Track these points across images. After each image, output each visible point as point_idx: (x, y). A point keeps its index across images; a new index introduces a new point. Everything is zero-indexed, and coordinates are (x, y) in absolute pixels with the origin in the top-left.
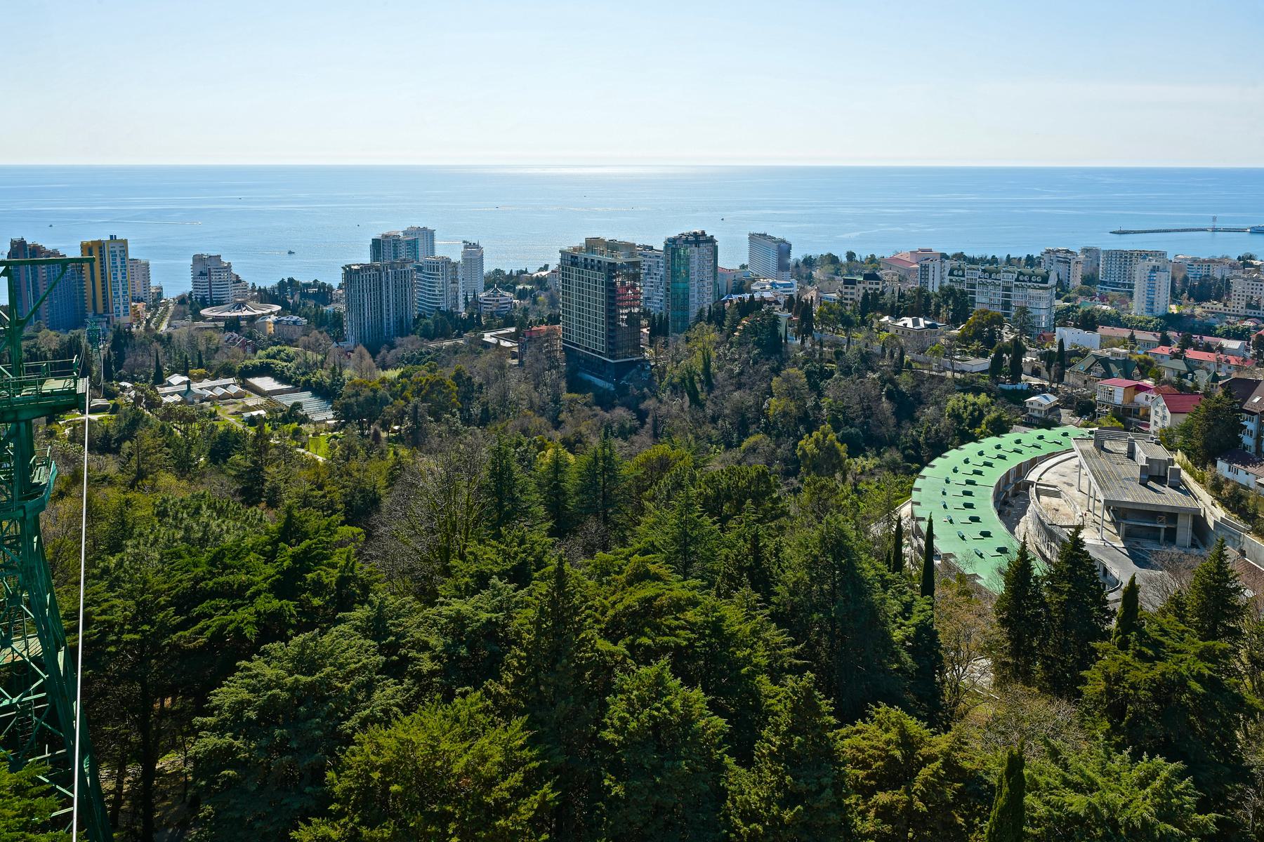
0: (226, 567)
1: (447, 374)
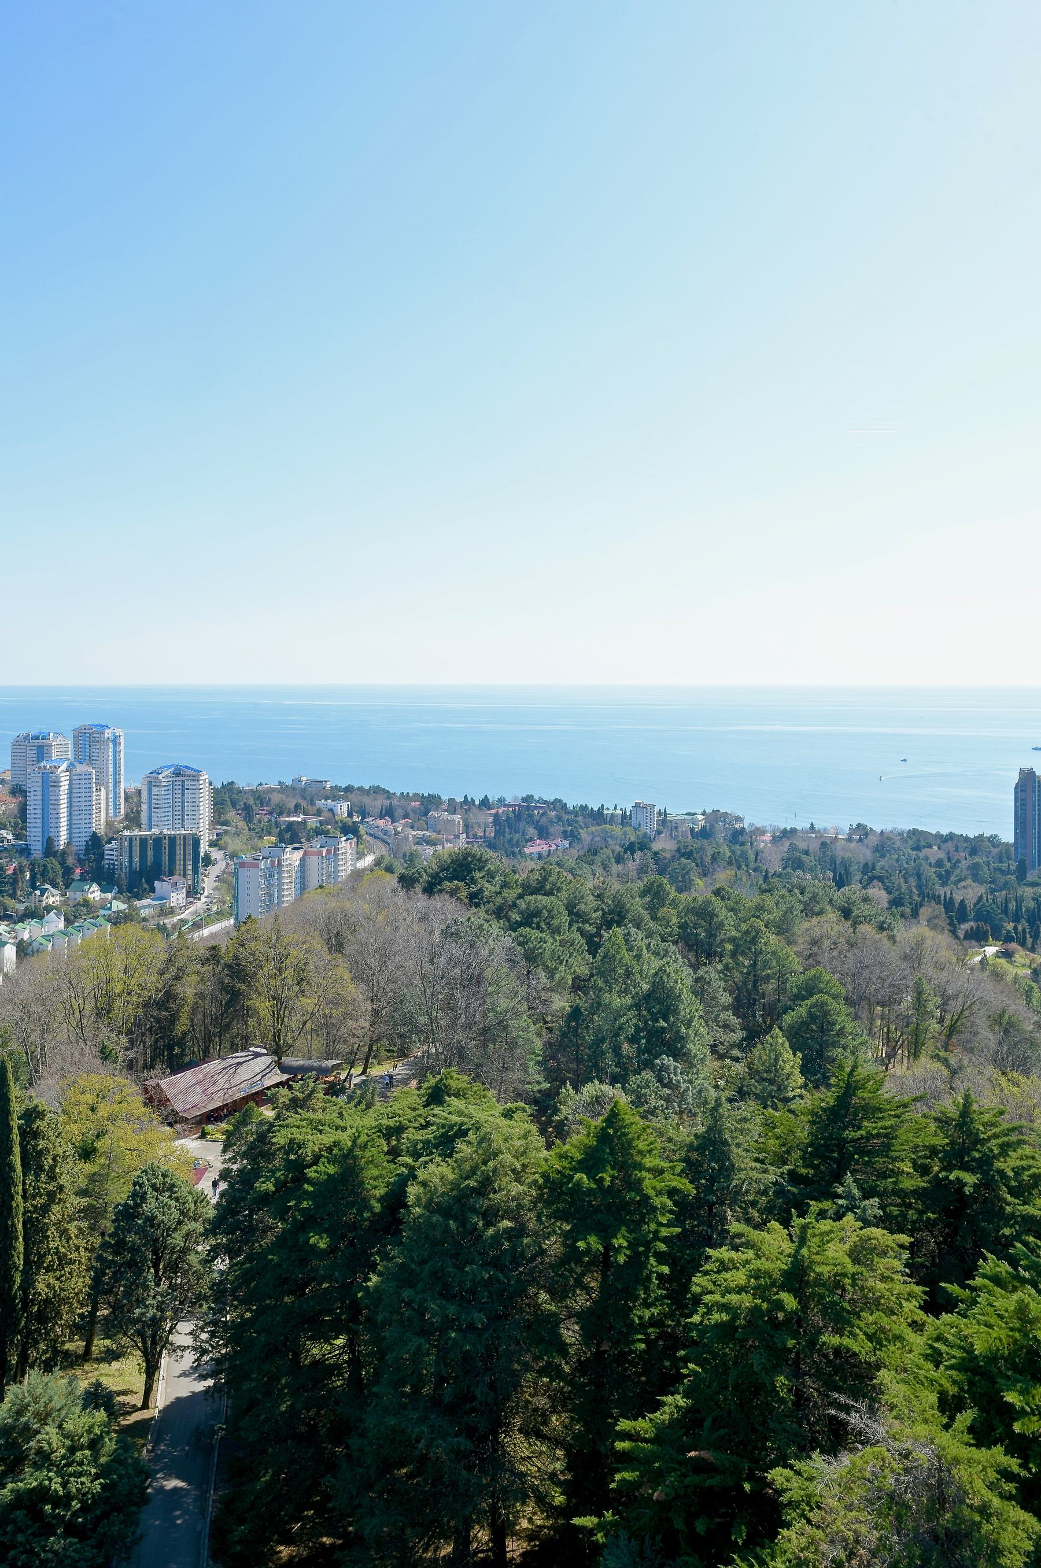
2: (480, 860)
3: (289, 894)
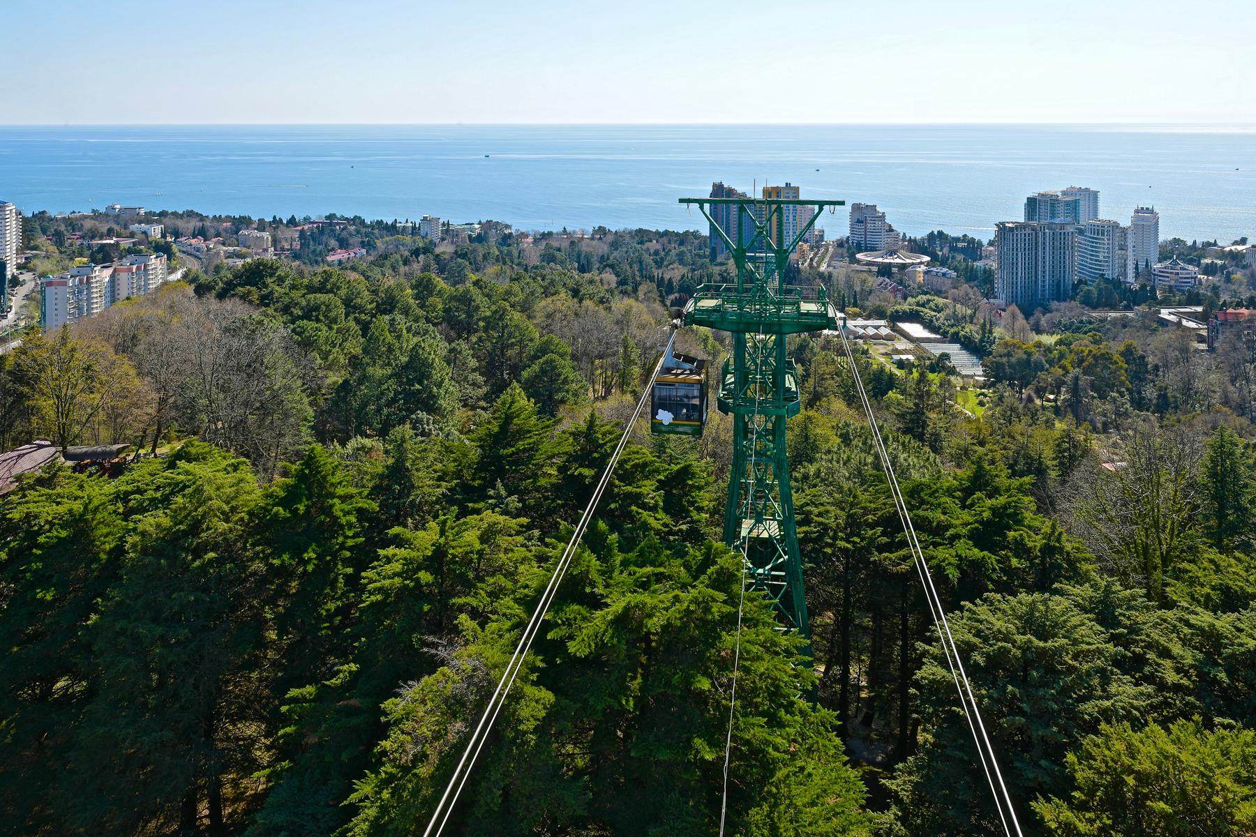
0: (923, 502)
1: (1115, 349)
2: (271, 267)
3: (98, 306)
